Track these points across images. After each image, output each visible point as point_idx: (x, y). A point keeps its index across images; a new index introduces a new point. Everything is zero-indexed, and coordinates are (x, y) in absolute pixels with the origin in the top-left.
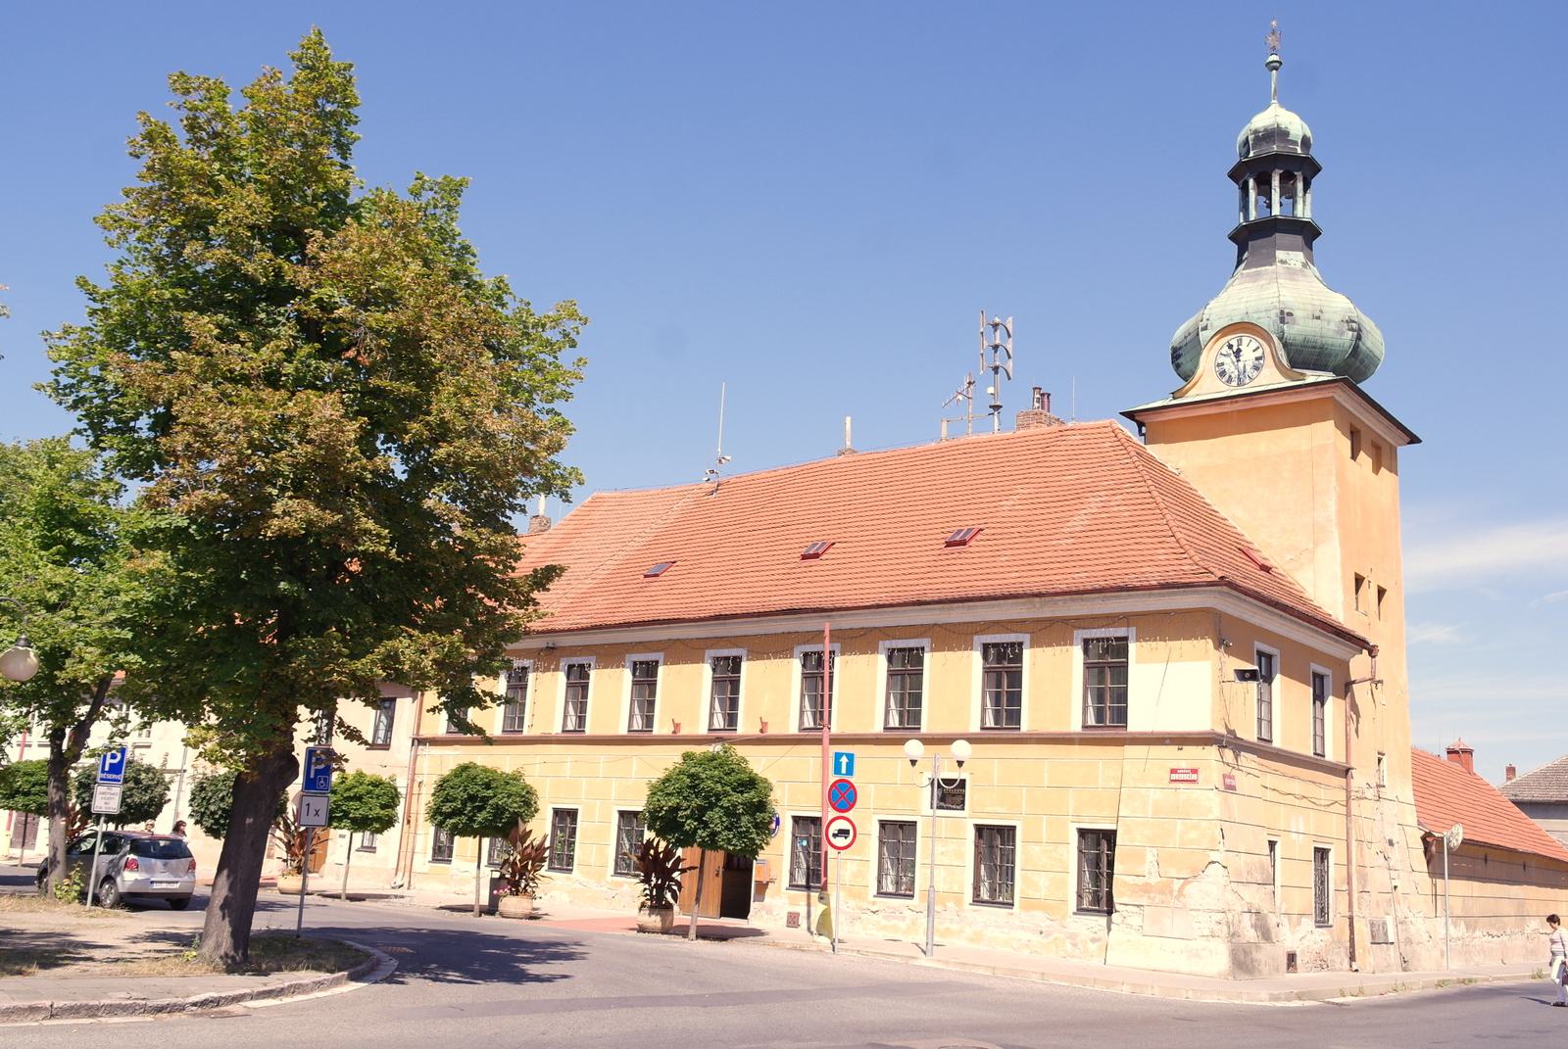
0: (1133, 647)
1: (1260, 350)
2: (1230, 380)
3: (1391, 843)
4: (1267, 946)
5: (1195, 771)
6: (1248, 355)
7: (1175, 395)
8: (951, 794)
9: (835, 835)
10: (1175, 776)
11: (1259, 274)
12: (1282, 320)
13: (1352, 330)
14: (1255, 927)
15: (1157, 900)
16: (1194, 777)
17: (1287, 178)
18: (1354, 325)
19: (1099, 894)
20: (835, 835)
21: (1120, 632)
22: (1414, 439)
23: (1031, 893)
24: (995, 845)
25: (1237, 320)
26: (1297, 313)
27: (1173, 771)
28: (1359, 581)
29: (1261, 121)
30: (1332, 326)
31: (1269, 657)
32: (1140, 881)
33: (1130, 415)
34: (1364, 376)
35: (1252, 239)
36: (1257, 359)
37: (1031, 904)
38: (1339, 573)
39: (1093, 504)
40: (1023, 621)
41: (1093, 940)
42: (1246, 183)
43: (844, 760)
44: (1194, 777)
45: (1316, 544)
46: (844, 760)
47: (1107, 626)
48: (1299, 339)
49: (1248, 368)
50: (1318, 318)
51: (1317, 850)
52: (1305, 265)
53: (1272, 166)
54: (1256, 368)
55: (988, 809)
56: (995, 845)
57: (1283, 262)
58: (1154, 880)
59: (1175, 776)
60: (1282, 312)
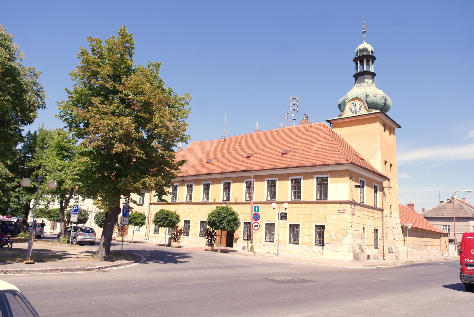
0: (329, 179)
1: (361, 105)
2: (353, 112)
3: (393, 228)
4: (362, 254)
5: (344, 210)
6: (358, 106)
7: (339, 116)
8: (283, 216)
9: (254, 227)
10: (339, 212)
11: (360, 85)
12: (366, 97)
13: (384, 99)
14: (359, 249)
15: (335, 242)
16: (344, 212)
17: (368, 61)
18: (385, 98)
19: (321, 242)
20: (254, 227)
21: (326, 176)
22: (399, 127)
23: (303, 241)
24: (294, 229)
25: (355, 97)
26: (370, 95)
27: (339, 210)
28: (386, 162)
29: (361, 47)
30: (379, 98)
31: (363, 182)
32: (331, 238)
33: (328, 121)
34: (387, 111)
35: (359, 76)
36: (360, 107)
37: (304, 244)
38: (381, 161)
39: (319, 144)
40: (301, 173)
41: (319, 252)
42: (357, 62)
43: (257, 208)
44: (344, 212)
45: (375, 153)
46: (257, 208)
47: (322, 174)
48: (371, 102)
49: (358, 109)
50: (375, 96)
51: (375, 230)
52: (372, 83)
53: (364, 58)
54: (360, 109)
55: (293, 220)
56: (294, 229)
57: (367, 82)
58: (334, 237)
59: (339, 212)
60: (366, 95)
